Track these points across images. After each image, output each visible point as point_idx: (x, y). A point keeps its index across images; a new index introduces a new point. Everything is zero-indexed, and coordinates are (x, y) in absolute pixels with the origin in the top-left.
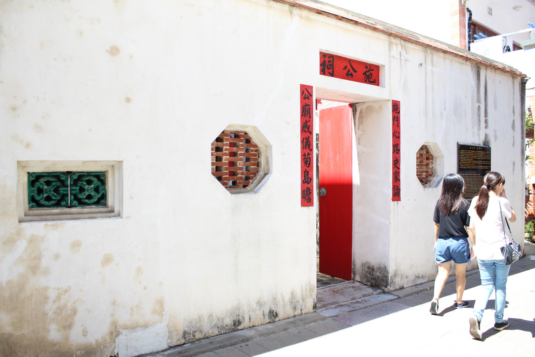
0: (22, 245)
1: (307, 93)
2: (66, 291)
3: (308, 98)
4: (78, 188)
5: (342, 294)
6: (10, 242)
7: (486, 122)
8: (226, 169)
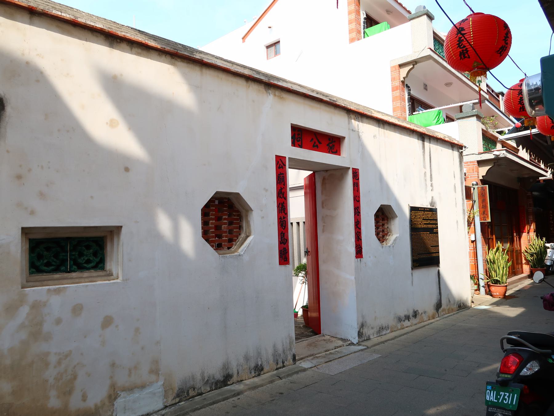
0: (24, 311)
1: (281, 163)
2: (67, 356)
3: (282, 167)
4: (77, 253)
5: (316, 346)
6: (11, 309)
7: (432, 185)
8: (213, 232)
